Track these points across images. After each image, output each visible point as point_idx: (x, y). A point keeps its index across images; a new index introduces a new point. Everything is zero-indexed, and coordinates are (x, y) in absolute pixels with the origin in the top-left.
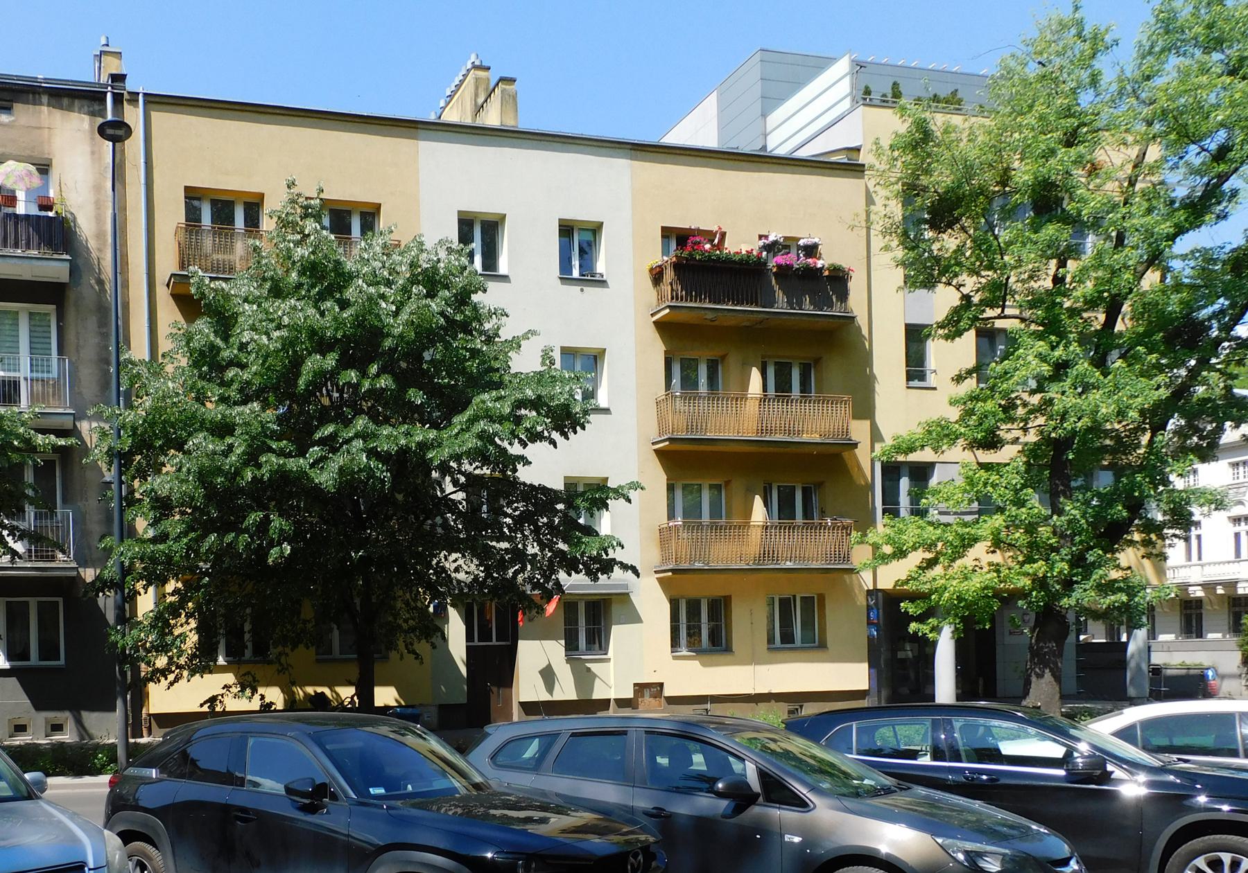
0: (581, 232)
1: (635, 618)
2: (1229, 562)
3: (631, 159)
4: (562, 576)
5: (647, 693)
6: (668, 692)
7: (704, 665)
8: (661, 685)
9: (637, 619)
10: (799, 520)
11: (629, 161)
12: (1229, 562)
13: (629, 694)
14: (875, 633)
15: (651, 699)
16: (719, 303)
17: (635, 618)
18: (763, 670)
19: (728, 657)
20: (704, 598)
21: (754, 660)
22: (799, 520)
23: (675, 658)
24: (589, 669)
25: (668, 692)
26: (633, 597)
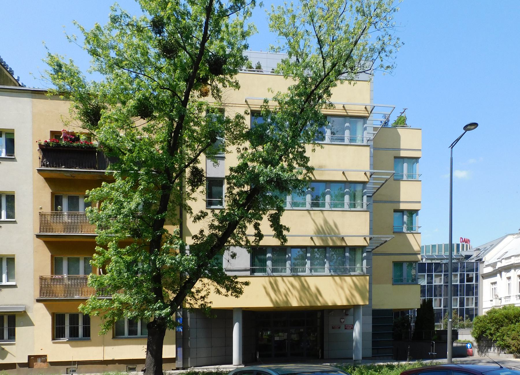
0: (7, 135)
1: (30, 323)
2: (11, 354)
3: (32, 98)
4: (277, 212)
5: (39, 360)
6: (49, 360)
7: (72, 346)
8: (46, 356)
9: (30, 324)
10: (346, 207)
11: (31, 99)
12: (11, 354)
13: (26, 361)
14: (182, 330)
15: (41, 363)
16: (70, 168)
17: (30, 323)
18: (108, 349)
19: (88, 343)
20: (67, 313)
21: (103, 343)
22: (346, 207)
23: (54, 343)
24: (3, 349)
25: (49, 360)
26: (29, 314)
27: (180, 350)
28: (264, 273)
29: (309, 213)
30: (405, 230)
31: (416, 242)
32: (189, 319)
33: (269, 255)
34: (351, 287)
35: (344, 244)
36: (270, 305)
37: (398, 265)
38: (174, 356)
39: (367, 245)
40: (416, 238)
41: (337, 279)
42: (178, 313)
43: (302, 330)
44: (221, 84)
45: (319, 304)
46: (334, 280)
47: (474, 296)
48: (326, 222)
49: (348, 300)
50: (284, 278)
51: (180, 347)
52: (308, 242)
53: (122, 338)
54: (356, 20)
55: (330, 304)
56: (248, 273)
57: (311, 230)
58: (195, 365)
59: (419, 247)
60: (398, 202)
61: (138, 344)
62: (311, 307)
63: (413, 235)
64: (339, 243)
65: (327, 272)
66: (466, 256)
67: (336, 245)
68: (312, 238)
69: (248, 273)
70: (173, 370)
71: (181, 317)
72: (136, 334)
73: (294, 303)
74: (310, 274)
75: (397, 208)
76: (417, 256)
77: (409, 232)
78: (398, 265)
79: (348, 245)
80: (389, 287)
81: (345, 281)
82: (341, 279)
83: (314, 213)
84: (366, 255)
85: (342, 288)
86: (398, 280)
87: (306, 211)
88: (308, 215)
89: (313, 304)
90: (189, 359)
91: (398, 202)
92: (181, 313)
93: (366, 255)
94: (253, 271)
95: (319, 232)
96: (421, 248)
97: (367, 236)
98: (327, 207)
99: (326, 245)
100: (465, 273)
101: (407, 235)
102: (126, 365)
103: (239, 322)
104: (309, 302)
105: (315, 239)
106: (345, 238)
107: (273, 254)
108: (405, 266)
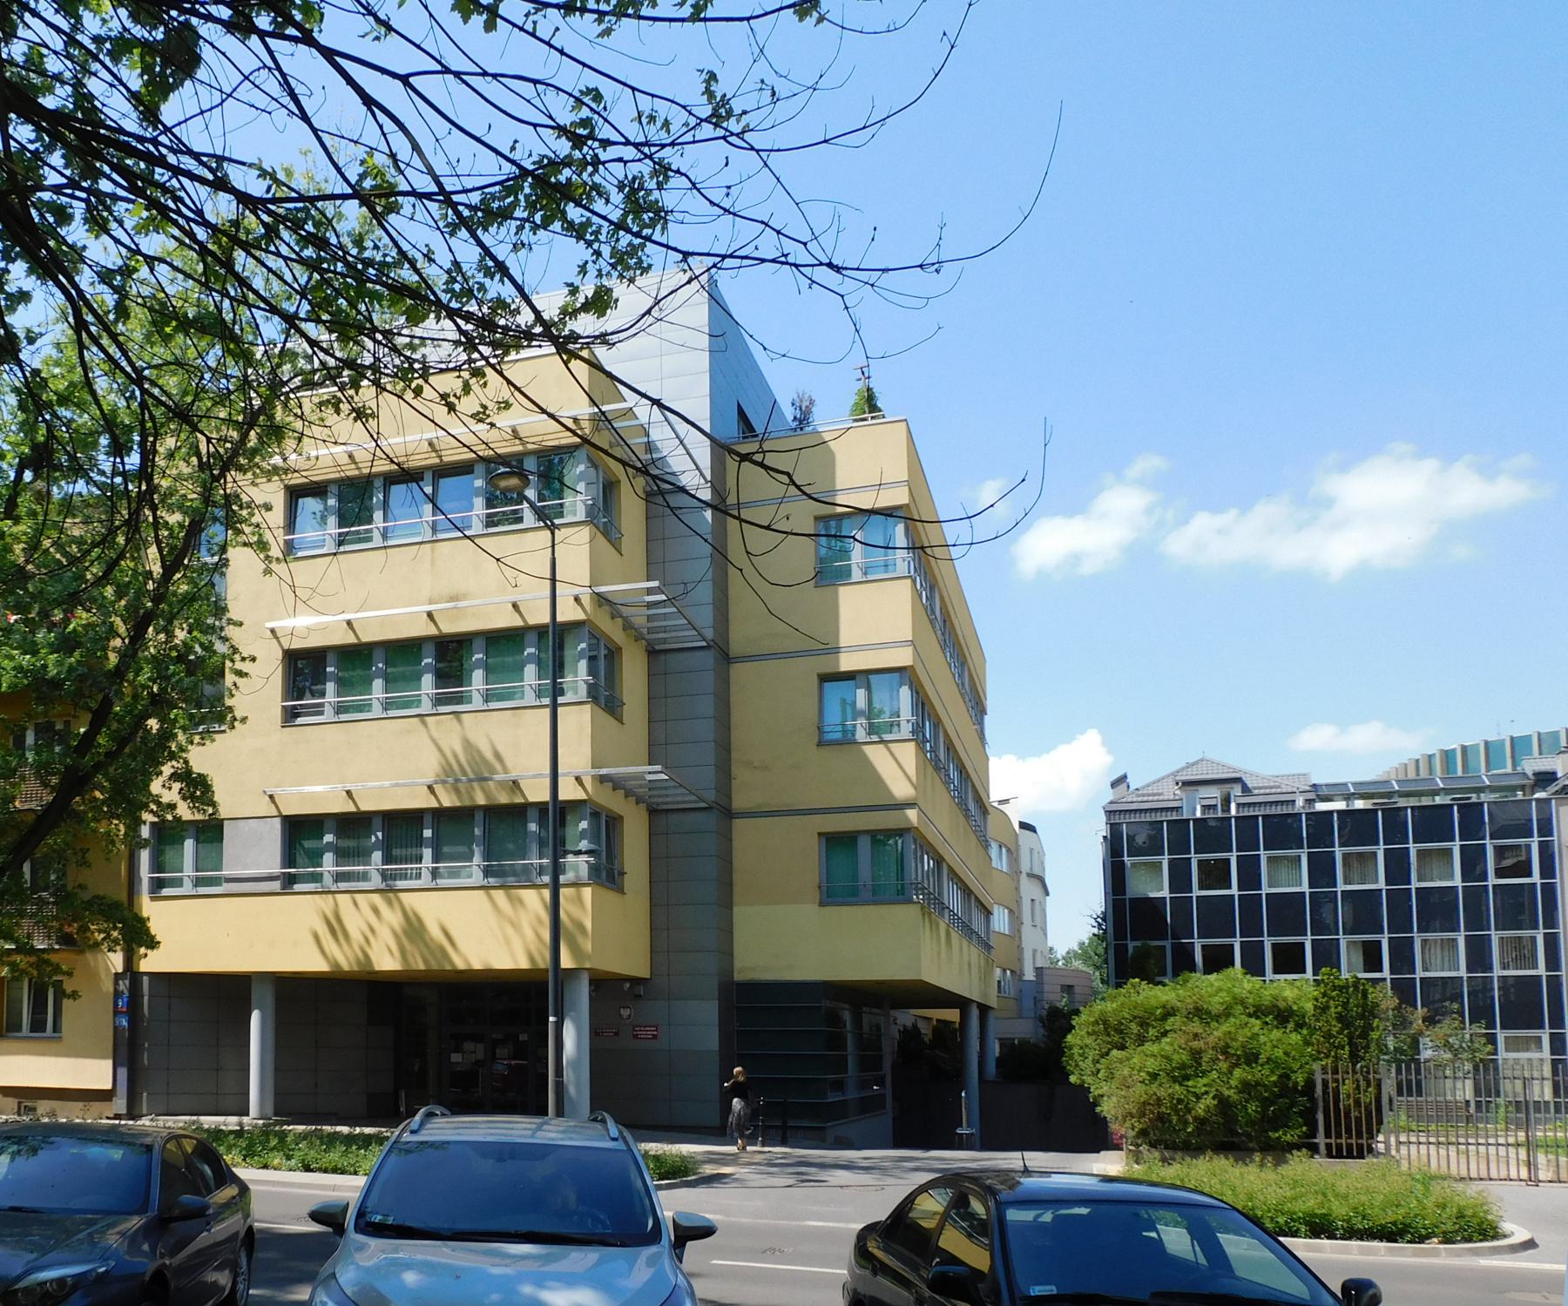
27: (123, 1073)
28: (318, 885)
29: (424, 723)
30: (861, 735)
31: (899, 770)
32: (146, 998)
33: (328, 838)
34: (540, 921)
35: (519, 800)
36: (318, 965)
37: (838, 843)
38: (109, 1086)
39: (584, 797)
40: (897, 756)
41: (499, 895)
42: (121, 982)
43: (523, 1037)
44: (299, 384)
45: (461, 965)
46: (490, 898)
47: (1536, 927)
48: (468, 745)
49: (532, 959)
50: (358, 897)
51: (122, 1065)
52: (423, 801)
53: (18, 1038)
54: (693, 94)
55: (477, 966)
56: (276, 886)
57: (429, 766)
58: (159, 1112)
59: (909, 785)
60: (834, 651)
61: (43, 1054)
62: (427, 972)
63: (889, 750)
64: (503, 799)
65: (477, 877)
66: (1540, 777)
67: (497, 802)
68: (430, 787)
69: (276, 886)
70: (108, 1118)
71: (126, 992)
72: (44, 1031)
73: (386, 961)
74: (432, 885)
75: (829, 670)
76: (904, 813)
77: (875, 738)
78: (838, 843)
79: (531, 799)
80: (808, 914)
81: (521, 902)
82: (509, 897)
83: (438, 723)
84: (586, 826)
85: (516, 926)
86: (835, 892)
87: (416, 719)
88: (421, 727)
89: (435, 966)
90: (145, 1094)
91: (834, 651)
92: (127, 982)
93: (586, 826)
94: (289, 882)
95: (450, 776)
96: (915, 788)
97: (587, 774)
98: (477, 701)
99: (467, 803)
100: (1487, 841)
101: (867, 749)
102: (16, 1100)
103: (261, 1011)
104: (425, 961)
105: (438, 789)
106: (523, 784)
107: (338, 835)
108: (864, 844)
